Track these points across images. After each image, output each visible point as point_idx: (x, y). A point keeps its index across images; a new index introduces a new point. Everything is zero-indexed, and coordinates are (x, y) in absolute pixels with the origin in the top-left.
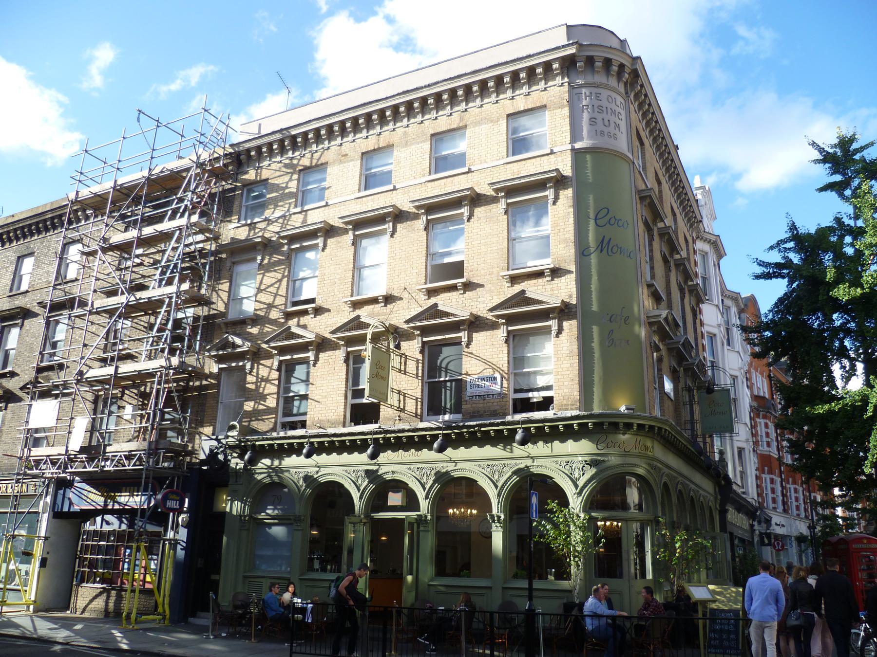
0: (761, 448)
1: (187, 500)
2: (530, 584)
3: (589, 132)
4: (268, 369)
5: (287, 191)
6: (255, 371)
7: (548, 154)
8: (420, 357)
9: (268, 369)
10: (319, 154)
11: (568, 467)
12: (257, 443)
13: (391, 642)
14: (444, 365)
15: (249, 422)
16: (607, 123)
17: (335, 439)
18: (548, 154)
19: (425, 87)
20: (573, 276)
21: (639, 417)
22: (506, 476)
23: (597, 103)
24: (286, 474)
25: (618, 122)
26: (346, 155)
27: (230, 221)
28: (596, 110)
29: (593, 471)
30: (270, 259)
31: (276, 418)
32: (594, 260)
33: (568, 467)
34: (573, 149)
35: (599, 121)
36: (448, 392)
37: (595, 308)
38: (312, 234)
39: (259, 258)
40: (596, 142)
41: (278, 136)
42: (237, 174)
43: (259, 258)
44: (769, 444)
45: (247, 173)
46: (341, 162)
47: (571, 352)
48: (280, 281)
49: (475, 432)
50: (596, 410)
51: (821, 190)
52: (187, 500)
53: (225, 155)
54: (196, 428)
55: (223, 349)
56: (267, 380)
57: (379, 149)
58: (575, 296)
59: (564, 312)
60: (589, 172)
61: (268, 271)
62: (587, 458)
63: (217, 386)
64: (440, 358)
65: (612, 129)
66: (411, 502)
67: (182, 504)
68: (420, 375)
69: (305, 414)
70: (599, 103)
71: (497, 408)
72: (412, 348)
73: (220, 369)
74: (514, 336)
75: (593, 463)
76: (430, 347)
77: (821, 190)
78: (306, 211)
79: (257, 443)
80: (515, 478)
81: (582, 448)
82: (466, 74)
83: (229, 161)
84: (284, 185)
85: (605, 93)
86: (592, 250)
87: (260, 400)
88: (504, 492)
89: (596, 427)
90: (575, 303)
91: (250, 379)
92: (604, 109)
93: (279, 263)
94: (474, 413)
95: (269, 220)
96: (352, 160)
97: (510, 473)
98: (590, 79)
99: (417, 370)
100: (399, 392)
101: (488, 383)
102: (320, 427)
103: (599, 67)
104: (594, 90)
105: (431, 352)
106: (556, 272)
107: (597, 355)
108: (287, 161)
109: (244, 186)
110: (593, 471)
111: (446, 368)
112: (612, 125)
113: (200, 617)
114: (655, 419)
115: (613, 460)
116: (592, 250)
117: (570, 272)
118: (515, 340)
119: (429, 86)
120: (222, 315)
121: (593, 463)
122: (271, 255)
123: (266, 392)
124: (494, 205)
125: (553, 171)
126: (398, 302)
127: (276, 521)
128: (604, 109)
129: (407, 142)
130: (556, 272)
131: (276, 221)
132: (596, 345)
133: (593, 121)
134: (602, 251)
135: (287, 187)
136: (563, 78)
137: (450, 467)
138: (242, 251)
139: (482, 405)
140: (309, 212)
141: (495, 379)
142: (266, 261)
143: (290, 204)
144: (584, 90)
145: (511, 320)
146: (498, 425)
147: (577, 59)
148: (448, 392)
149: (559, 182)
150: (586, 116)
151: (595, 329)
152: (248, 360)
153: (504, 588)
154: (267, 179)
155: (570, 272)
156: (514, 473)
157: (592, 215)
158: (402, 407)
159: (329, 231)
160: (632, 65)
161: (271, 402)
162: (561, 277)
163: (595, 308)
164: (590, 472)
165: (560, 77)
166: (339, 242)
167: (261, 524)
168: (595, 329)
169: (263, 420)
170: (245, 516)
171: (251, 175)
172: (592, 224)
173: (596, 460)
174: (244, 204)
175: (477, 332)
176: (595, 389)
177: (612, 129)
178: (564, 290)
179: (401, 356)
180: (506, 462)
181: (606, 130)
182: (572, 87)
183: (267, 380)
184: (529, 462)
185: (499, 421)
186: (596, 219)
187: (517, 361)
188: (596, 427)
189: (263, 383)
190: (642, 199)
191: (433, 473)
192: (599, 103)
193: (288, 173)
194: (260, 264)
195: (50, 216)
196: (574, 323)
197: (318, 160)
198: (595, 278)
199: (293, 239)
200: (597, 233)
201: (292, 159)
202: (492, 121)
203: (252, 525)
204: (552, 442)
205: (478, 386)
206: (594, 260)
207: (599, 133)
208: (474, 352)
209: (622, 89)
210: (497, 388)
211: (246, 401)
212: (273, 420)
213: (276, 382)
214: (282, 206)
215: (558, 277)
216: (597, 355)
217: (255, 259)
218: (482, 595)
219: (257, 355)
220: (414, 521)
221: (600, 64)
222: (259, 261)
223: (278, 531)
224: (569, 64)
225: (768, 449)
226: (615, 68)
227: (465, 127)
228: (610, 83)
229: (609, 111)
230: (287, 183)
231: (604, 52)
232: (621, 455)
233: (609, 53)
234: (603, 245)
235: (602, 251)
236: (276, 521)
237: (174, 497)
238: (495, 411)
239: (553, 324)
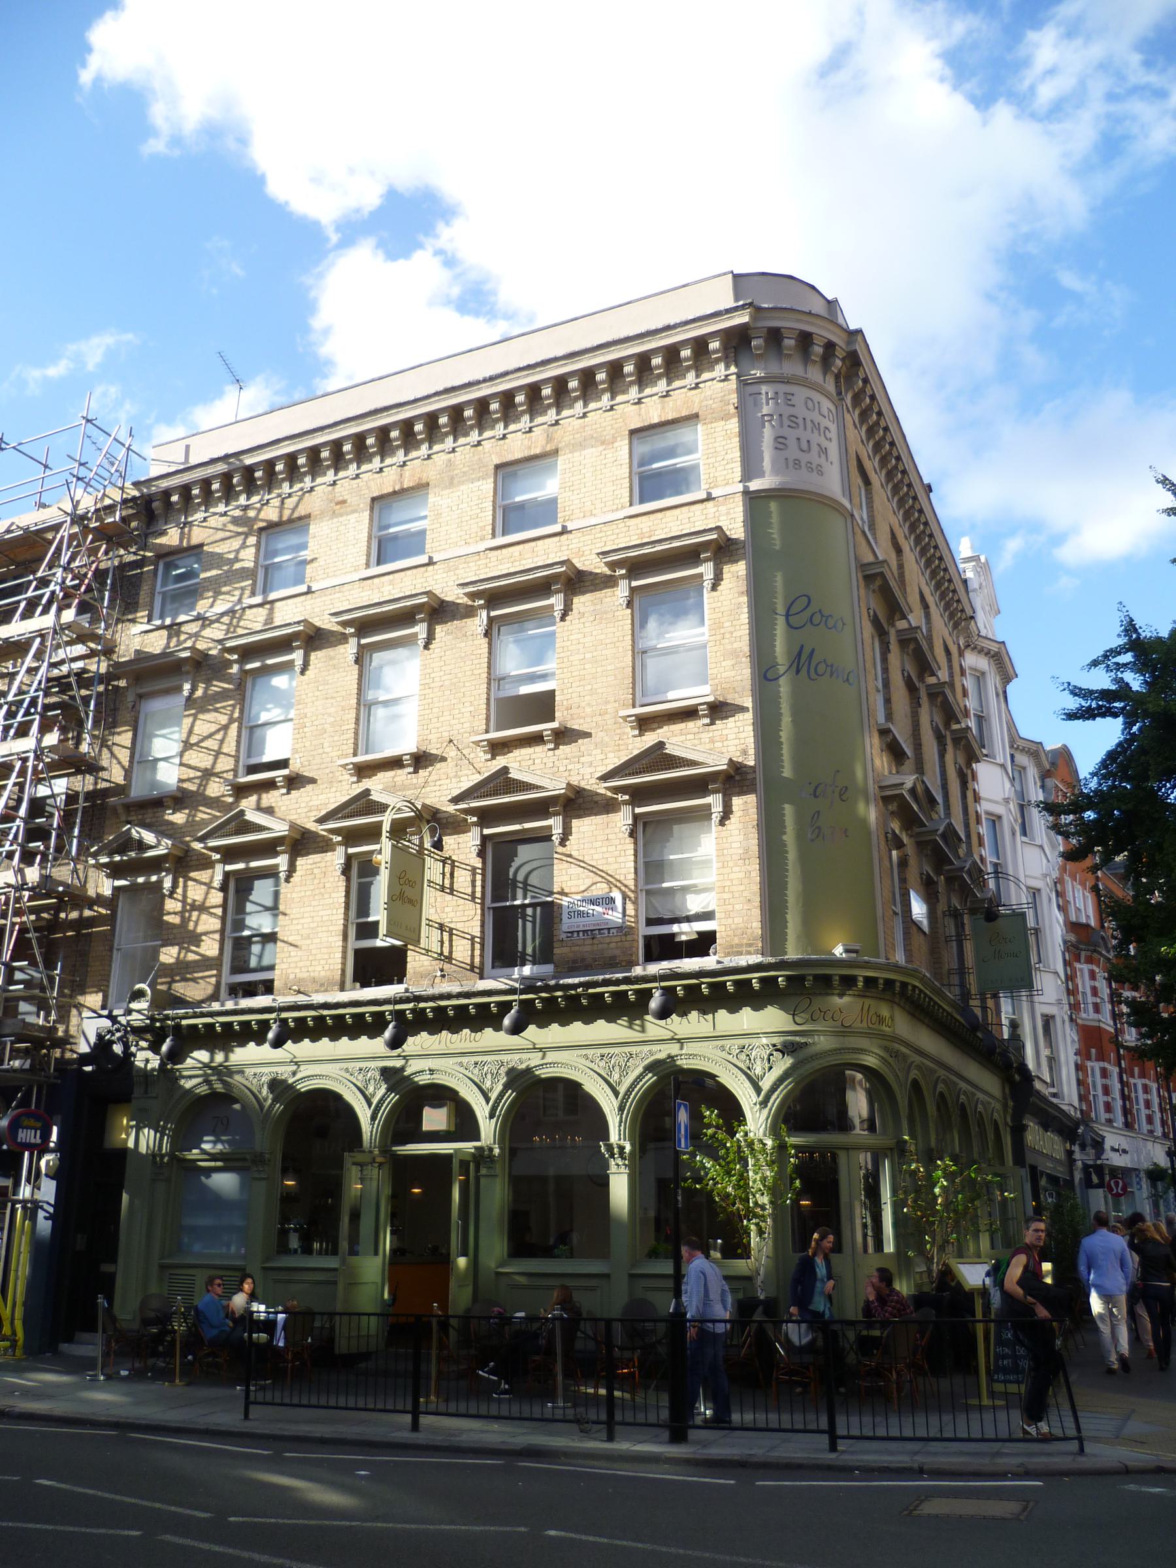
1: (55, 1129)
3: (774, 462)
4: (204, 888)
5: (237, 566)
6: (180, 890)
7: (702, 501)
8: (478, 863)
9: (204, 888)
10: (295, 499)
11: (743, 1057)
12: (184, 1022)
14: (520, 877)
15: (170, 983)
16: (805, 446)
17: (325, 1012)
18: (702, 501)
19: (485, 380)
20: (749, 716)
21: (867, 965)
22: (633, 1075)
23: (788, 411)
24: (238, 1077)
27: (133, 621)
28: (786, 422)
29: (788, 1062)
30: (206, 689)
31: (219, 976)
32: (784, 687)
33: (743, 1057)
34: (746, 493)
35: (792, 442)
36: (529, 925)
37: (787, 772)
38: (283, 645)
39: (187, 687)
40: (786, 479)
41: (221, 468)
42: (147, 536)
43: (187, 687)
45: (164, 533)
47: (747, 851)
48: (225, 728)
49: (578, 996)
50: (792, 955)
52: (55, 1129)
53: (125, 501)
54: (71, 997)
55: (121, 852)
56: (202, 908)
58: (752, 751)
59: (733, 780)
60: (775, 532)
61: (203, 710)
62: (777, 1040)
63: (111, 919)
64: (515, 865)
65: (814, 456)
67: (46, 1136)
68: (478, 895)
69: (271, 968)
70: (791, 411)
71: (617, 952)
72: (464, 847)
73: (116, 889)
74: (645, 824)
75: (787, 1049)
78: (272, 602)
79: (184, 1022)
80: (650, 1079)
81: (767, 1021)
82: (556, 359)
83: (131, 511)
84: (232, 556)
85: (801, 393)
86: (782, 669)
87: (191, 943)
88: (631, 1104)
89: (790, 985)
90: (752, 763)
91: (171, 905)
92: (800, 421)
93: (223, 695)
94: (574, 961)
95: (205, 619)
97: (640, 1069)
98: (775, 368)
99: (474, 886)
100: (441, 927)
101: (599, 909)
102: (299, 992)
103: (789, 348)
105: (499, 854)
106: (719, 710)
107: (792, 855)
108: (237, 513)
109: (159, 557)
110: (788, 1062)
111: (525, 883)
112: (815, 448)
115: (823, 1043)
116: (782, 669)
117: (743, 709)
118: (646, 831)
119: (491, 379)
120: (120, 790)
121: (787, 1049)
122: (208, 682)
123: (200, 929)
124: (608, 591)
125: (711, 530)
126: (438, 765)
127: (219, 1164)
130: (719, 710)
131: (217, 621)
132: (789, 838)
133: (780, 442)
134: (798, 672)
135: (237, 560)
136: (727, 367)
137: (534, 1060)
138: (155, 674)
139: (588, 948)
140: (278, 604)
141: (613, 900)
142: (199, 693)
143: (243, 589)
144: (764, 388)
146: (617, 982)
147: (752, 333)
148: (529, 925)
149: (723, 549)
150: (768, 434)
151: (788, 809)
152: (168, 871)
153: (632, 1276)
154: (201, 545)
155: (743, 709)
156: (649, 1068)
157: (781, 609)
158: (446, 953)
159: (314, 639)
160: (848, 343)
161: (210, 947)
162: (726, 718)
163: (787, 772)
164: (783, 1064)
165: (722, 366)
166: (331, 658)
167: (192, 1169)
168: (788, 809)
169: (194, 980)
170: (162, 1156)
171: (171, 537)
172: (781, 622)
173: (792, 1043)
174: (158, 588)
175: (579, 817)
176: (789, 917)
177: (814, 456)
178: (732, 742)
179: (444, 862)
180: (634, 1049)
181: (804, 458)
182: (743, 383)
183: (202, 908)
184: (674, 1049)
185: (620, 976)
186: (787, 615)
187: (651, 868)
188: (790, 985)
189: (195, 914)
190: (869, 579)
191: (503, 1070)
192: (791, 411)
193: (239, 534)
194: (189, 698)
196: (751, 799)
197: (294, 510)
198: (786, 720)
199: (248, 652)
200: (789, 640)
201: (246, 508)
202: (603, 443)
203: (176, 1171)
204: (714, 1012)
205: (581, 914)
206: (784, 687)
207: (791, 464)
208: (574, 854)
209: (831, 387)
210: (615, 917)
211: (163, 946)
212: (213, 980)
213: (219, 911)
214: (228, 593)
215: (722, 719)
216: (792, 855)
217: (179, 689)
218: (593, 1289)
219: (183, 863)
220: (468, 1158)
221: (792, 342)
222: (186, 693)
223: (225, 1182)
224: (737, 343)
228: (809, 375)
229: (809, 424)
230: (237, 551)
231: (798, 321)
232: (836, 1034)
233: (808, 323)
234: (801, 660)
235: (798, 672)
236: (219, 1164)
237: (32, 1122)
238: (613, 958)
239: (714, 801)
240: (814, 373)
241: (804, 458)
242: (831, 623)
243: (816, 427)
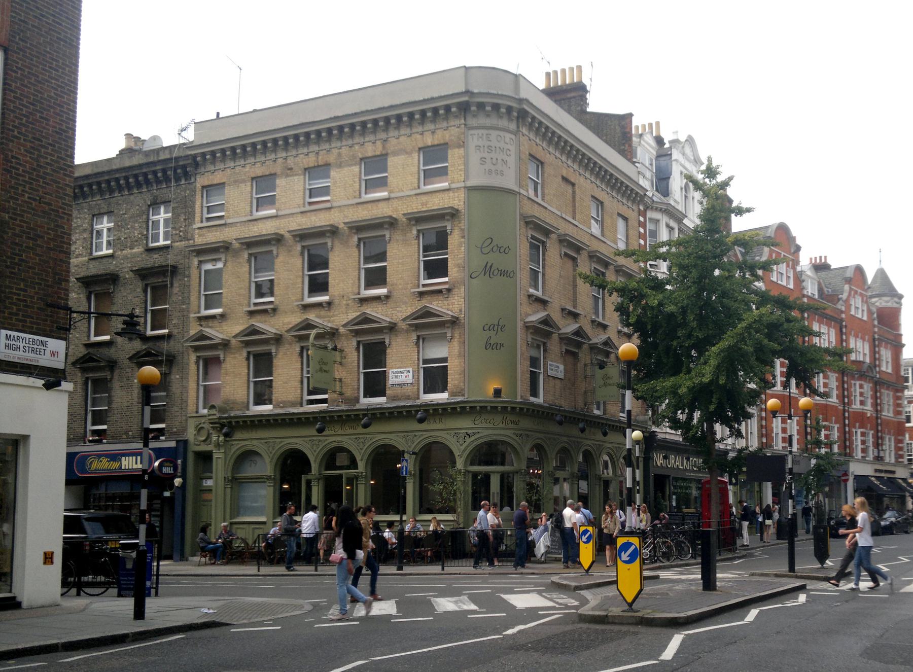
0: (854, 406)
2: (401, 518)
13: (682, 574)
16: (494, 160)
25: (505, 158)
26: (291, 169)
28: (486, 150)
35: (488, 161)
44: (862, 403)
46: (287, 176)
51: (749, 210)
57: (318, 166)
66: (353, 464)
76: (364, 345)
77: (749, 210)
85: (494, 133)
92: (493, 149)
96: (296, 175)
104: (485, 132)
113: (528, 568)
114: (520, 403)
128: (493, 149)
129: (341, 163)
145: (417, 327)
181: (493, 168)
195: (106, 178)
225: (862, 407)
226: (503, 110)
227: (387, 154)
229: (499, 161)
237: (168, 464)
240: (504, 123)
241: (493, 168)
242: (502, 250)
243: (502, 150)
